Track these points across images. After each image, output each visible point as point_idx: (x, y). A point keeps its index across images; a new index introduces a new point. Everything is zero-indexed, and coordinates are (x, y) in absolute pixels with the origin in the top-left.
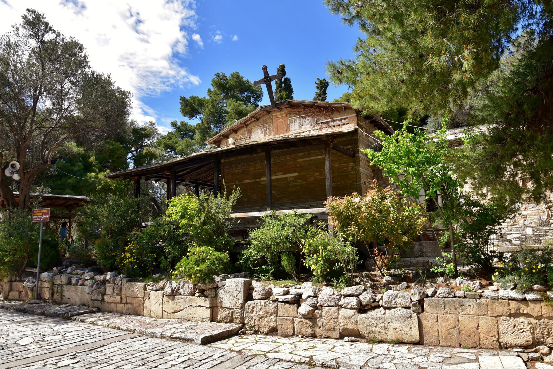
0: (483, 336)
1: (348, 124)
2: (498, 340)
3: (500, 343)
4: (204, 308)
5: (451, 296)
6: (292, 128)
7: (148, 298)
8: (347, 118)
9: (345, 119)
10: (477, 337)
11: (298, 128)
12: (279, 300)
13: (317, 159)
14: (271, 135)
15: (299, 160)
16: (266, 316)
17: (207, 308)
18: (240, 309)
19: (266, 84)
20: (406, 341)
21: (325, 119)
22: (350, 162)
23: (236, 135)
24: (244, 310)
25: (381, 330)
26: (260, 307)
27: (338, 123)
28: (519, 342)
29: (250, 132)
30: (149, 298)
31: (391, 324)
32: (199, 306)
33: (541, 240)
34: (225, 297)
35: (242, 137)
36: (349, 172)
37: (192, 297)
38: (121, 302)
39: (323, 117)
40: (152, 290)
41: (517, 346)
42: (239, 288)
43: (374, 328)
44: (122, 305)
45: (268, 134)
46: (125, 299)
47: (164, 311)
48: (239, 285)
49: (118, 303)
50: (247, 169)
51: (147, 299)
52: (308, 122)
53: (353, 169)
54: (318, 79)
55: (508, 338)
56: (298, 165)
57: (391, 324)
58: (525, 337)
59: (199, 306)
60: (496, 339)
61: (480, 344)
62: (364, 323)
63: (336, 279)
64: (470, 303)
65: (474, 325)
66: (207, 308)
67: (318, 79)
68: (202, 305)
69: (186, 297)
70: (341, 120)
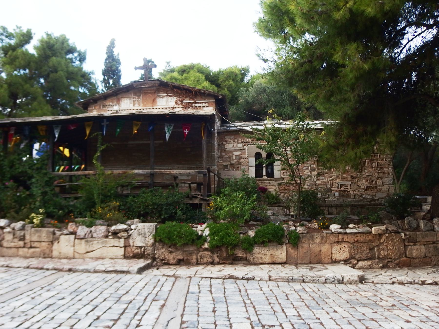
0: (323, 256)
2: (331, 258)
3: (332, 259)
4: (118, 248)
5: (306, 232)
9: (205, 103)
10: (320, 256)
14: (139, 106)
17: (121, 247)
18: (151, 247)
20: (278, 262)
21: (189, 100)
24: (155, 247)
25: (262, 256)
27: (200, 105)
28: (342, 258)
32: (113, 246)
33: (326, 201)
34: (138, 238)
37: (106, 239)
38: (24, 247)
39: (188, 98)
40: (61, 234)
41: (342, 261)
43: (257, 255)
44: (25, 250)
45: (137, 105)
46: (29, 244)
48: (151, 228)
49: (20, 247)
54: (136, 68)
55: (337, 256)
58: (346, 255)
59: (113, 246)
60: (330, 257)
61: (321, 261)
64: (317, 236)
65: (318, 249)
66: (121, 247)
67: (136, 68)
68: (116, 245)
69: (99, 239)
70: (203, 103)
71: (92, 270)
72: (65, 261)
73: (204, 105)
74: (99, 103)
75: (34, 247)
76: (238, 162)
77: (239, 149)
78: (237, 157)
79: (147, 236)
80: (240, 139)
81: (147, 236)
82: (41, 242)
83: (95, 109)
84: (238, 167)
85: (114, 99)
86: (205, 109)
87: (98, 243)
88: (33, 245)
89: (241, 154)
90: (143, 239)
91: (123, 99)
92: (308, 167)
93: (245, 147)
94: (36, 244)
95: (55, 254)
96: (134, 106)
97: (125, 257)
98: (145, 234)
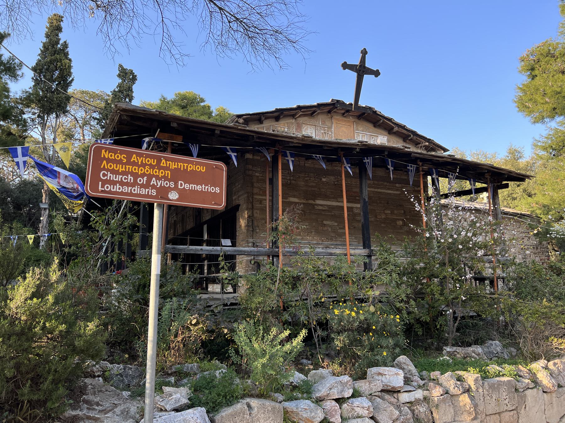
7: (524, 406)
19: (357, 65)
23: (277, 123)
35: (286, 130)
50: (293, 182)
51: (523, 411)
85: (293, 123)
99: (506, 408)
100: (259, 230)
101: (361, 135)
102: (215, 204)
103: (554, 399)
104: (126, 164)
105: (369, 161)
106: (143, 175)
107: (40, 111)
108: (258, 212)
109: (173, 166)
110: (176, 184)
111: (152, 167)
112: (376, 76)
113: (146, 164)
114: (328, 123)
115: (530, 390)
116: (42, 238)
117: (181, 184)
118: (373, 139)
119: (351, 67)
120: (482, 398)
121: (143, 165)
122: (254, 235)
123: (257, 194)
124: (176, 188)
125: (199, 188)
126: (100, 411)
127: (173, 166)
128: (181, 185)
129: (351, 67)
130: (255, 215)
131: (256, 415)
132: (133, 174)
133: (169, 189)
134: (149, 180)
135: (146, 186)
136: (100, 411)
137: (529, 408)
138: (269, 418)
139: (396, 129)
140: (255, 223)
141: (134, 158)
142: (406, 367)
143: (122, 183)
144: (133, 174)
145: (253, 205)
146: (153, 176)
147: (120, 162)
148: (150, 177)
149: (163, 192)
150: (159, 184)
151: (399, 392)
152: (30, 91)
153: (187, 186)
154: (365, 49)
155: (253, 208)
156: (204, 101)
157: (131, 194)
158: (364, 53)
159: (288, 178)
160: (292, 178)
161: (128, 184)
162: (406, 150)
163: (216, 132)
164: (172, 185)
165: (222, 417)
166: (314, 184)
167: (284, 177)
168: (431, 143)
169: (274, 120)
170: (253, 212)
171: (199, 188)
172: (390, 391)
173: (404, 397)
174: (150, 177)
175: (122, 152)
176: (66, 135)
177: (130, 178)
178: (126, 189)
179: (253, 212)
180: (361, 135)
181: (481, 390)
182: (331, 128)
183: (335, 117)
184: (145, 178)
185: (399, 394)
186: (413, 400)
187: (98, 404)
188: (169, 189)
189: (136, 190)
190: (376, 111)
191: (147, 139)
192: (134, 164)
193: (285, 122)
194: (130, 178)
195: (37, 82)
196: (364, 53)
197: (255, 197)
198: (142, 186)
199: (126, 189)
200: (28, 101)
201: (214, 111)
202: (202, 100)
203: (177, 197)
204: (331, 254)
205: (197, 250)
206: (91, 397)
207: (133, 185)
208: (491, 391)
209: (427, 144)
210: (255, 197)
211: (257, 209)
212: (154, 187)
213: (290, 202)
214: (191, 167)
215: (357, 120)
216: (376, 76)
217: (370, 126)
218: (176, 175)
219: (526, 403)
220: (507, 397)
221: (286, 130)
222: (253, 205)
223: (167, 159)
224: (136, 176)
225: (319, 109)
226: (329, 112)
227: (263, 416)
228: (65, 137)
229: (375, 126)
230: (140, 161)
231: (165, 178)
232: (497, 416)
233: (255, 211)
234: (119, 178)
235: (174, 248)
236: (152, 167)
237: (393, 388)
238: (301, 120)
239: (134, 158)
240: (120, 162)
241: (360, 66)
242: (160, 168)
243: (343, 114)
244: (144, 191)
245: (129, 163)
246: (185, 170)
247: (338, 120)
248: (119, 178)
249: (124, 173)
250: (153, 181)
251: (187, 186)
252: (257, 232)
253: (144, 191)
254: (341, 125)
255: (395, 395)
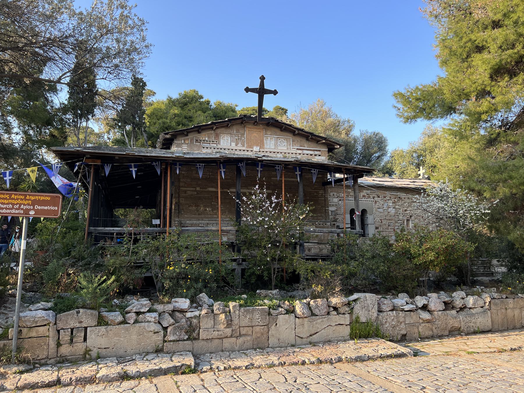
1: (320, 155)
6: (267, 145)
7: (275, 324)
8: (320, 151)
9: (317, 150)
11: (273, 147)
12: (405, 310)
13: (291, 181)
14: (243, 146)
15: (272, 178)
16: (398, 325)
19: (257, 89)
22: (320, 190)
23: (199, 134)
26: (392, 318)
29: (217, 136)
30: (276, 325)
31: (478, 319)
34: (361, 312)
35: (207, 139)
36: (319, 198)
42: (374, 302)
43: (470, 324)
44: (233, 340)
45: (240, 145)
47: (296, 337)
50: (212, 176)
51: (273, 327)
52: (284, 144)
53: (322, 195)
56: (272, 183)
57: (478, 319)
62: (464, 321)
63: (263, 276)
68: (341, 323)
71: (366, 358)
72: (476, 347)
73: (316, 153)
74: (191, 136)
75: (245, 335)
76: (334, 218)
77: (335, 204)
78: (333, 213)
79: (370, 308)
80: (335, 194)
81: (370, 308)
82: (252, 327)
83: (185, 143)
84: (334, 224)
85: (211, 134)
86: (317, 157)
87: (322, 321)
88: (243, 332)
89: (337, 210)
90: (366, 312)
91: (222, 136)
92: (399, 226)
93: (340, 202)
94: (244, 331)
95: (272, 341)
96: (236, 145)
97: (353, 336)
98: (368, 306)
99: (257, 324)
100: (184, 212)
101: (269, 138)
102: (54, 215)
103: (306, 323)
104: (8, 199)
105: (243, 165)
106: (17, 204)
107: (74, 117)
108: (183, 199)
109: (33, 198)
110: (34, 207)
111: (22, 199)
112: (275, 94)
113: (19, 199)
114: (241, 131)
115: (282, 315)
116: (80, 213)
117: (37, 207)
118: (280, 140)
119: (253, 90)
120: (237, 317)
121: (17, 199)
122: (180, 216)
123: (182, 187)
124: (34, 209)
125: (46, 208)
126: (9, 311)
127: (33, 198)
128: (37, 207)
129: (253, 90)
130: (181, 202)
131: (81, 316)
132: (12, 204)
133: (30, 210)
134: (20, 206)
135: (19, 209)
136: (9, 311)
137: (280, 325)
138: (89, 318)
139: (297, 132)
140: (181, 207)
141: (13, 196)
142: (203, 299)
143: (6, 209)
144: (12, 204)
145: (179, 195)
146: (22, 204)
147: (6, 199)
148: (20, 205)
149: (27, 212)
150: (25, 208)
151: (186, 312)
152: (66, 102)
153: (39, 208)
154: (263, 76)
155: (179, 197)
156: (203, 98)
157: (11, 213)
158: (262, 78)
159: (208, 174)
160: (211, 174)
161: (9, 209)
162: (259, 159)
163: (116, 158)
164: (32, 207)
165: (61, 315)
166: (229, 177)
167: (204, 173)
168: (328, 140)
169: (197, 132)
170: (179, 200)
171: (46, 208)
172: (181, 311)
173: (189, 315)
174: (20, 205)
175: (7, 194)
176: (110, 126)
177: (11, 206)
178: (8, 211)
179: (179, 200)
180: (269, 138)
181: (237, 312)
182: (244, 134)
183: (247, 126)
184: (18, 206)
185: (186, 313)
186: (193, 316)
187: (10, 308)
188: (30, 210)
189: (13, 211)
190: (278, 120)
191: (78, 164)
192: (13, 199)
193: (204, 133)
194: (11, 206)
195: (71, 94)
196: (262, 78)
197: (181, 189)
198: (16, 209)
199: (8, 211)
200: (64, 109)
201: (213, 105)
202: (201, 97)
203: (34, 213)
204: (207, 230)
205: (111, 230)
206: (7, 305)
207: (11, 209)
208: (245, 313)
209: (324, 141)
210: (181, 189)
211: (182, 197)
212: (22, 209)
213: (209, 191)
214: (42, 198)
215: (266, 127)
216: (275, 94)
217: (278, 131)
218: (34, 203)
219: (277, 322)
220: (260, 318)
221: (207, 139)
222: (179, 195)
223: (29, 195)
224: (13, 204)
225: (230, 123)
226: (242, 123)
227: (85, 316)
228: (109, 128)
229: (281, 131)
230: (16, 197)
231: (28, 204)
232: (251, 328)
233: (181, 199)
234: (5, 206)
235: (95, 229)
236: (22, 199)
237: (181, 309)
238: (219, 131)
239: (13, 196)
240: (6, 199)
241: (260, 89)
242: (26, 200)
243: (254, 123)
244: (17, 212)
245: (10, 199)
246: (39, 200)
247: (250, 128)
248: (5, 206)
249: (7, 204)
250: (22, 206)
251: (39, 208)
252: (182, 214)
253: (17, 212)
254: (253, 132)
255: (184, 314)
